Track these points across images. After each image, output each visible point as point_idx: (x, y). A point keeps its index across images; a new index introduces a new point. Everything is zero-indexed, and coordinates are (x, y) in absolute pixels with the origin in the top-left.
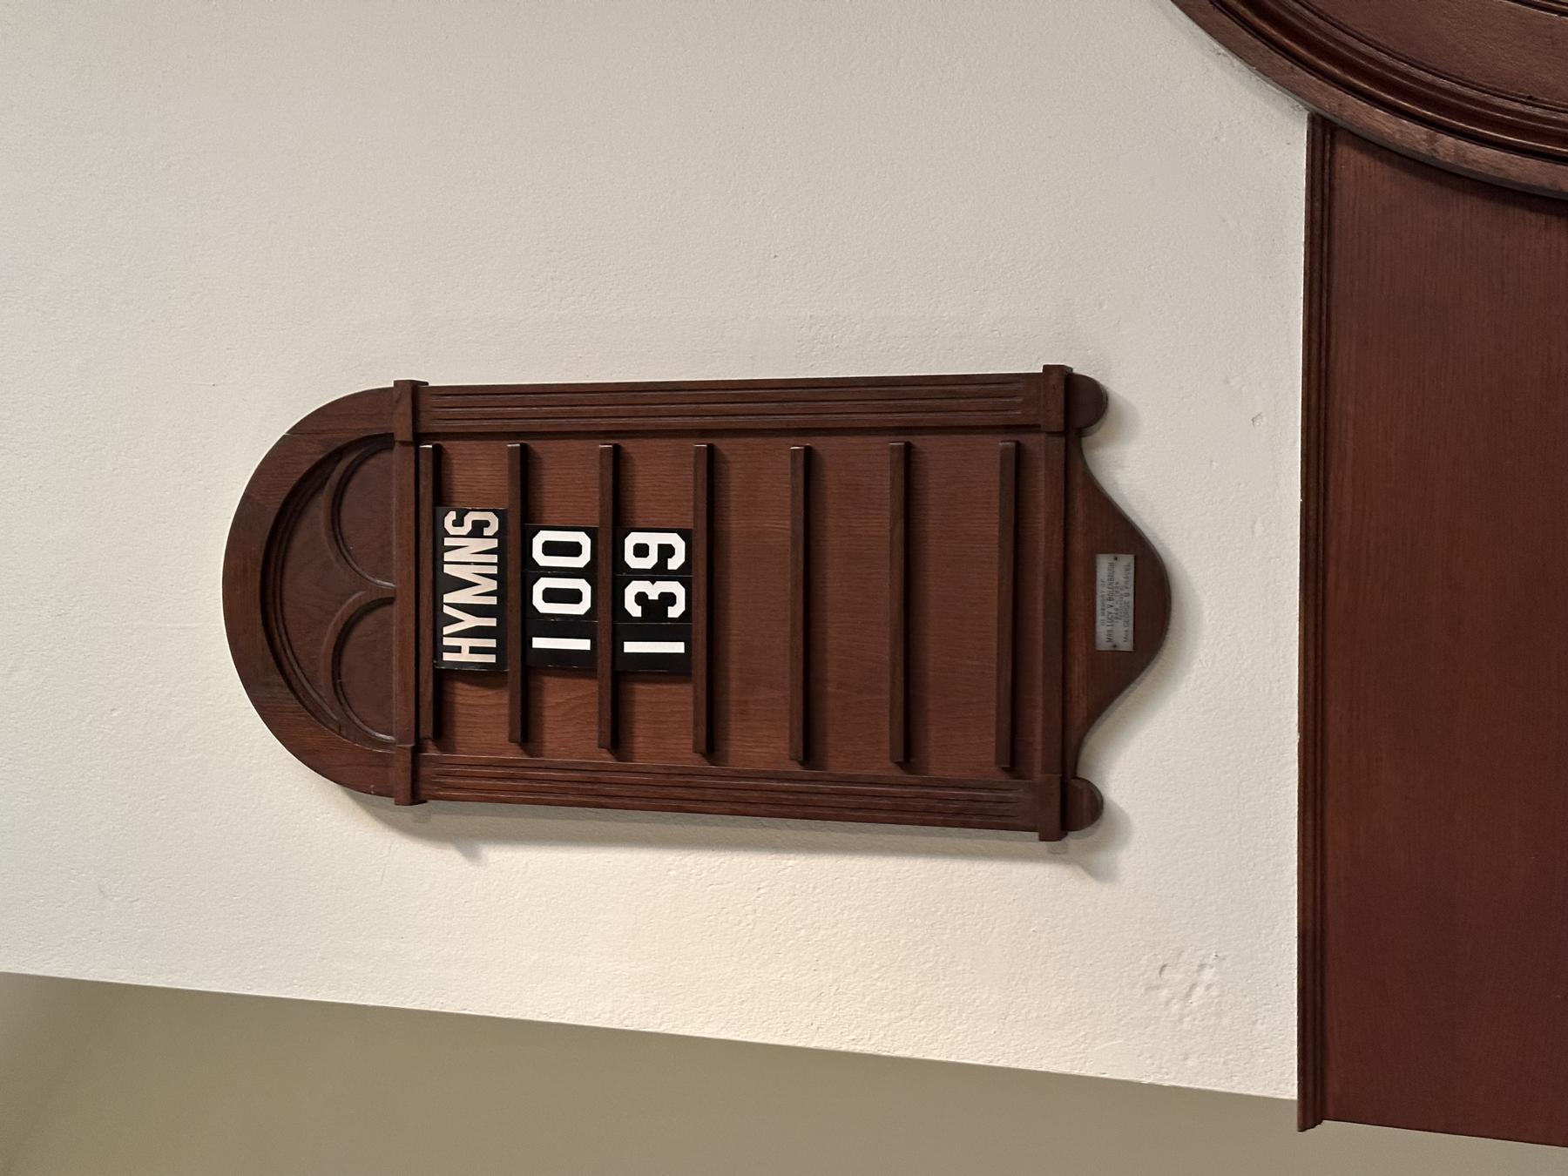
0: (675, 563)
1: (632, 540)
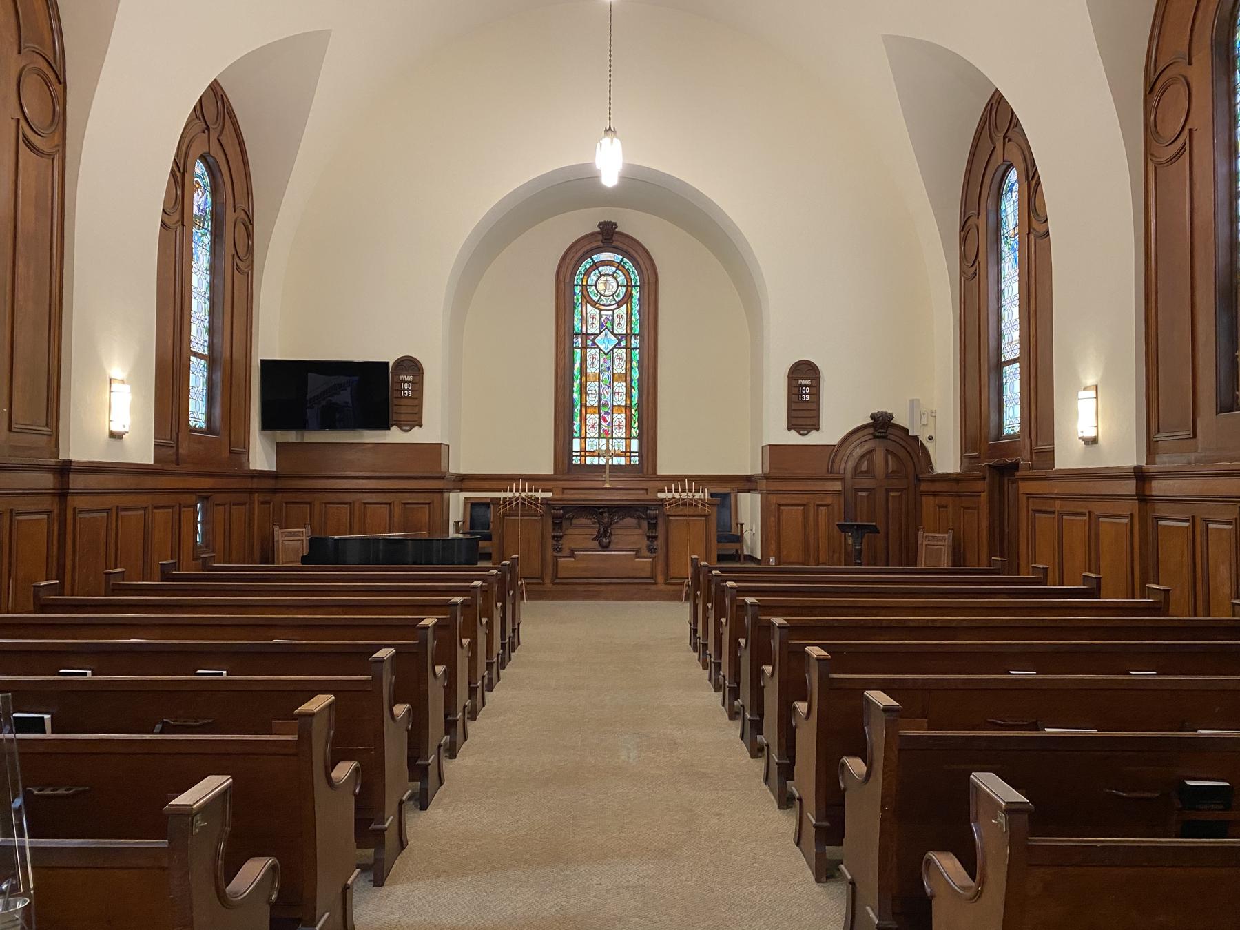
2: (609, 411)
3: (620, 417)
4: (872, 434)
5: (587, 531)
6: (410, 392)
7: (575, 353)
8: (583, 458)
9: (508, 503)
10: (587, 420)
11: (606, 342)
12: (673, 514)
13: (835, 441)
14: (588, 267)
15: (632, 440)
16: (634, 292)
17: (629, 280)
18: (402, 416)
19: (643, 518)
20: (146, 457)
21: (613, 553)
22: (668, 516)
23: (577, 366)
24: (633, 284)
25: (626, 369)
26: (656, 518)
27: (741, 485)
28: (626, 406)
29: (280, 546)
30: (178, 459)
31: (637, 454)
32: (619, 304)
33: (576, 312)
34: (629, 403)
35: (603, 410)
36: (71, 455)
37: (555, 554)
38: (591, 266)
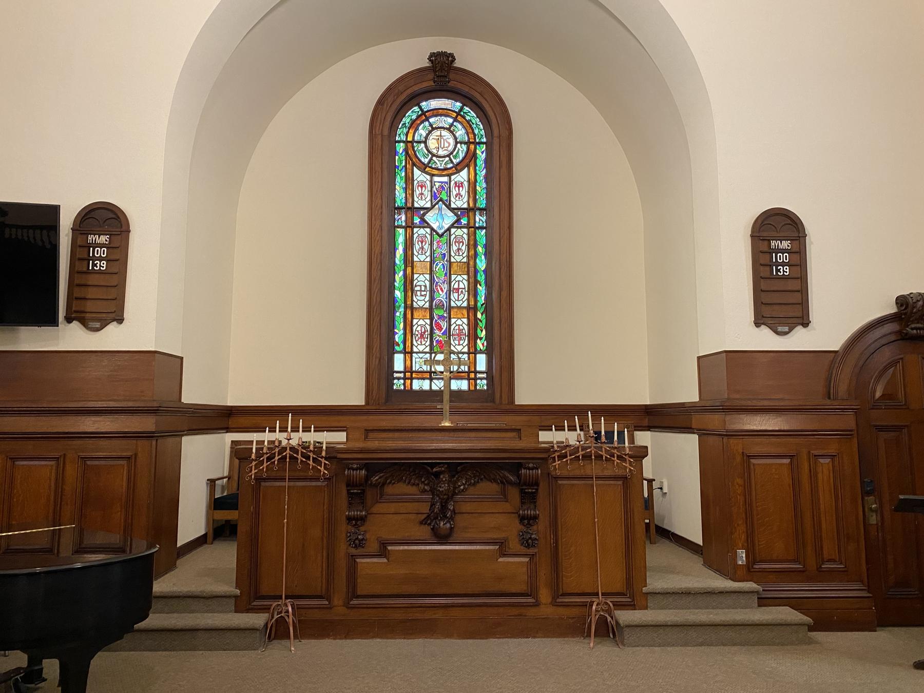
0: (101, 268)
1: (788, 267)
2: (445, 315)
3: (460, 323)
4: (896, 333)
5: (411, 507)
7: (397, 234)
8: (408, 382)
9: (265, 456)
10: (414, 328)
11: (441, 219)
12: (565, 473)
13: (835, 344)
14: (414, 117)
15: (478, 356)
16: (478, 152)
17: (471, 136)
19: (511, 483)
21: (457, 547)
22: (557, 478)
23: (400, 252)
24: (477, 140)
25: (468, 256)
26: (537, 484)
27: (536, 419)
28: (468, 308)
31: (484, 375)
32: (458, 168)
33: (398, 179)
34: (472, 303)
35: (437, 313)
37: (353, 551)
38: (418, 117)
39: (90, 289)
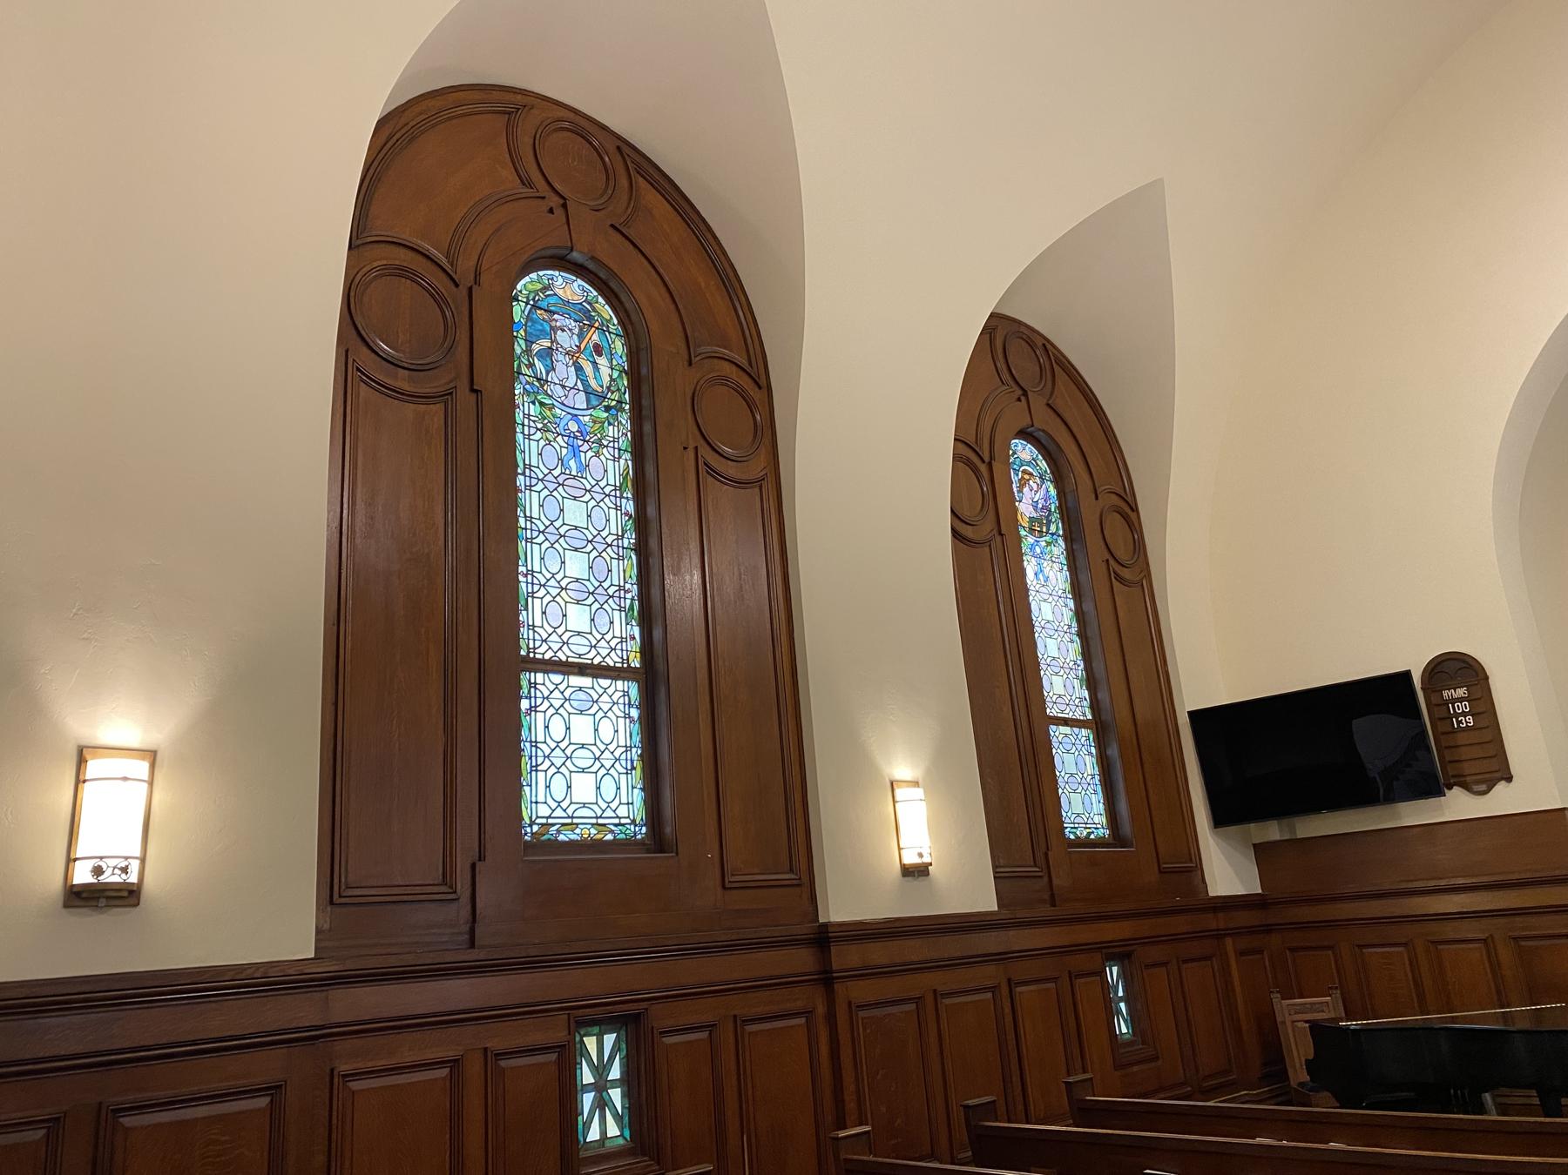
1: (1470, 717)
6: (1470, 719)
18: (1466, 765)
20: (983, 898)
29: (1290, 1031)
30: (1052, 896)
36: (831, 914)
39: (1463, 749)
